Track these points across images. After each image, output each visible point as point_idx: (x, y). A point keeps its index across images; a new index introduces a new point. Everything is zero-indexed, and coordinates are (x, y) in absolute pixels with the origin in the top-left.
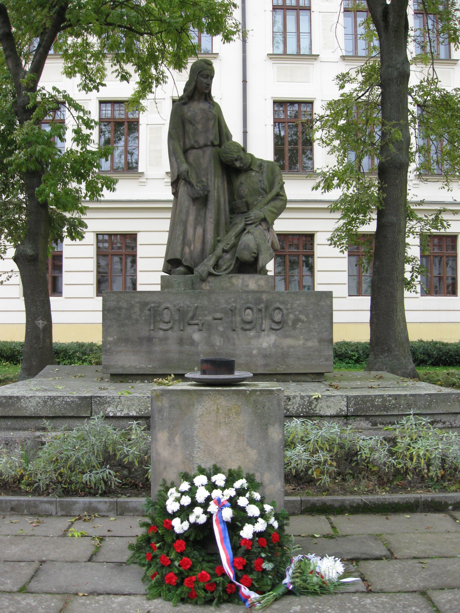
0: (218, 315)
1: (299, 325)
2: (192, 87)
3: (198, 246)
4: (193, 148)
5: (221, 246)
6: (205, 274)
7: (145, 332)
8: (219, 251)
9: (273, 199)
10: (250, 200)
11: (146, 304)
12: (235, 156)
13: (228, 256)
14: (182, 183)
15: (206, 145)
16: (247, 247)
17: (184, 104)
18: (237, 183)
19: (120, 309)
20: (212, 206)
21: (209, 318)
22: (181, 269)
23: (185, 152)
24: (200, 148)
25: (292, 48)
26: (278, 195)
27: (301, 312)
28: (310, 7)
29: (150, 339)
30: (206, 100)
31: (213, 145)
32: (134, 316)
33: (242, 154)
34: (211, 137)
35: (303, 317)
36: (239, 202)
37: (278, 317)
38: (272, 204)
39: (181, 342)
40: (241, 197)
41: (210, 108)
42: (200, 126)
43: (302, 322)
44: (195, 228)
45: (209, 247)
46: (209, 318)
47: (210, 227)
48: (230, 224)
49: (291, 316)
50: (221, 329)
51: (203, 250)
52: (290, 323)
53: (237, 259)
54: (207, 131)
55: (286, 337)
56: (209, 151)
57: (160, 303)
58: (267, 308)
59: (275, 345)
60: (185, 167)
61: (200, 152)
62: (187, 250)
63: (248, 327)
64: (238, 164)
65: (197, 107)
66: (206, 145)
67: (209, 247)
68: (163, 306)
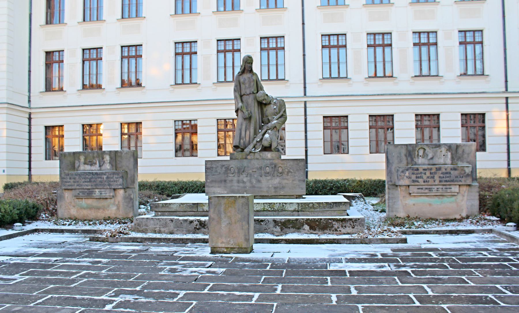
0: (254, 170)
1: (290, 174)
2: (243, 68)
3: (247, 139)
4: (244, 95)
5: (256, 140)
6: (248, 153)
7: (223, 177)
8: (255, 142)
9: (280, 117)
10: (270, 118)
11: (223, 166)
12: (263, 98)
13: (258, 144)
14: (239, 111)
15: (250, 94)
16: (266, 140)
17: (240, 75)
18: (265, 109)
19: (212, 168)
20: (253, 122)
21: (251, 171)
22: (239, 150)
23: (241, 96)
24: (248, 95)
25: (425, 72)
26: (282, 115)
27: (290, 168)
28: (346, 45)
29: (225, 181)
30: (250, 72)
31: (253, 93)
32: (218, 171)
33: (266, 97)
34: (253, 90)
35: (291, 170)
36: (265, 119)
37: (280, 170)
38: (280, 119)
39: (238, 182)
40: (267, 116)
41: (252, 76)
42: (247, 85)
43: (291, 172)
44: (246, 132)
45: (251, 139)
46: (251, 171)
47: (252, 131)
48: (261, 128)
49: (286, 170)
50: (256, 176)
51: (249, 141)
52: (286, 173)
53: (263, 145)
54: (250, 87)
55: (284, 179)
56: (252, 96)
57: (229, 165)
58: (275, 166)
59: (279, 183)
60: (240, 104)
61: (248, 96)
62: (242, 141)
63: (267, 175)
64: (264, 102)
65: (247, 76)
66: (250, 94)
67: (251, 139)
68: (231, 167)
